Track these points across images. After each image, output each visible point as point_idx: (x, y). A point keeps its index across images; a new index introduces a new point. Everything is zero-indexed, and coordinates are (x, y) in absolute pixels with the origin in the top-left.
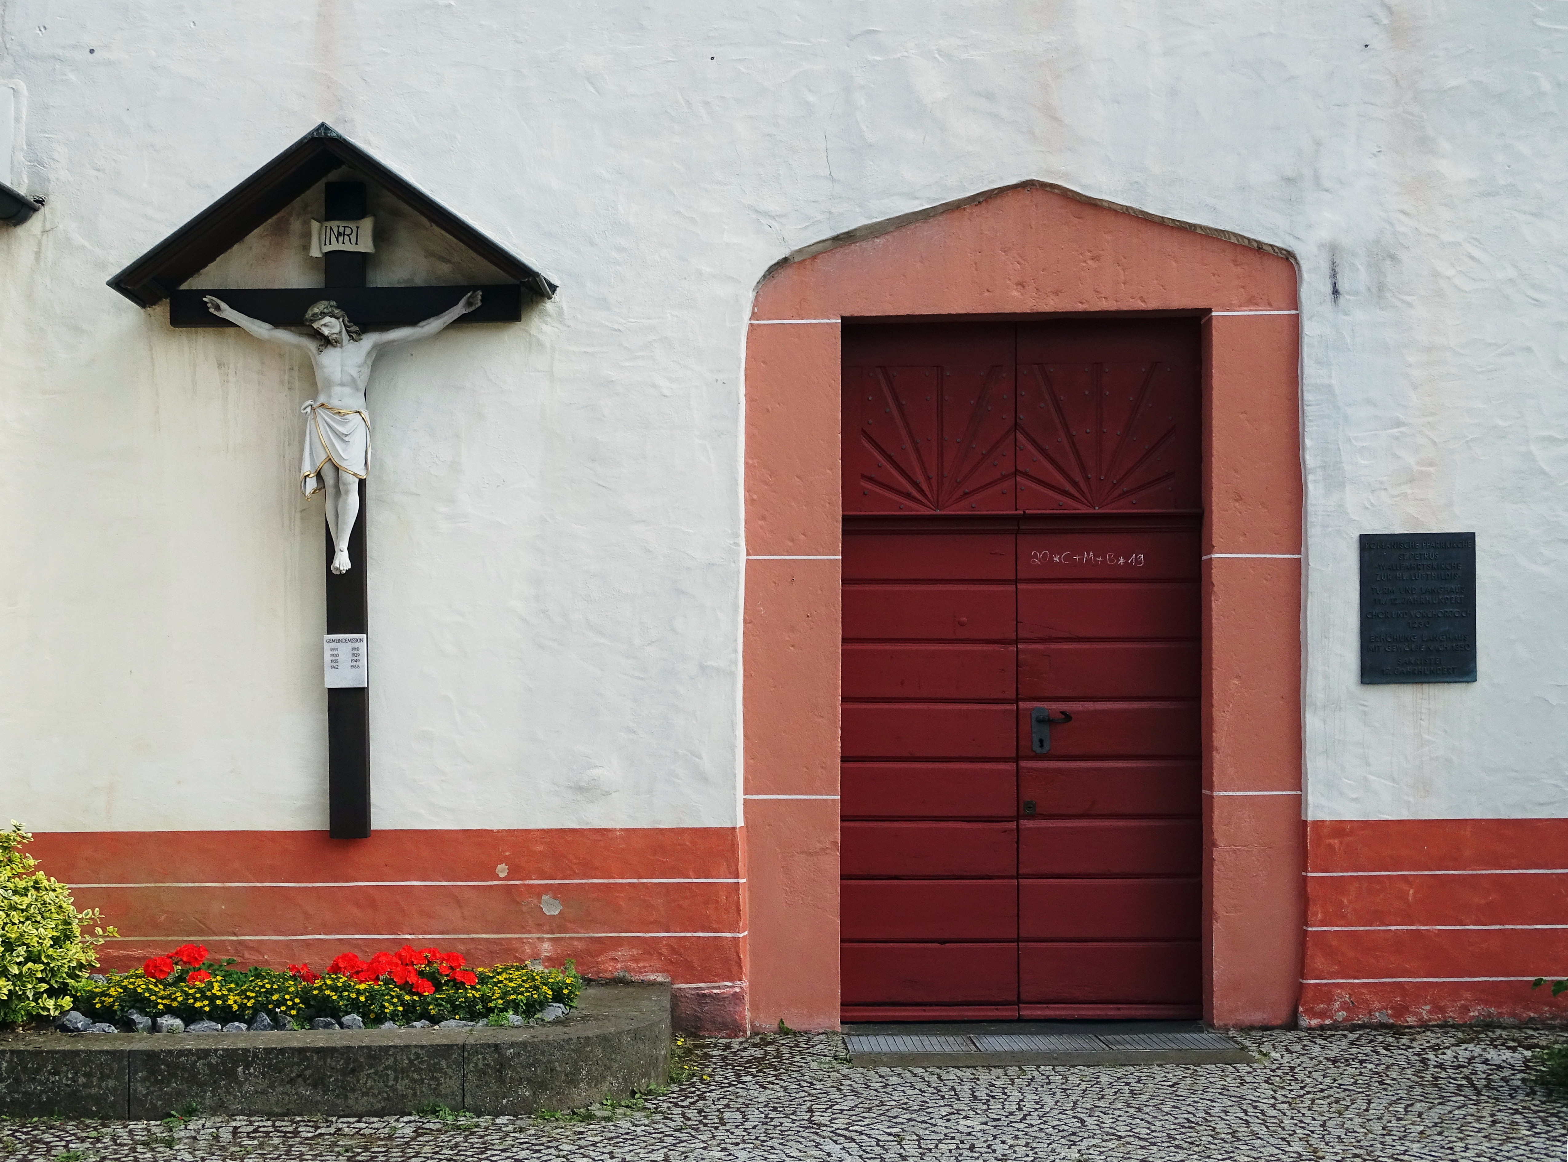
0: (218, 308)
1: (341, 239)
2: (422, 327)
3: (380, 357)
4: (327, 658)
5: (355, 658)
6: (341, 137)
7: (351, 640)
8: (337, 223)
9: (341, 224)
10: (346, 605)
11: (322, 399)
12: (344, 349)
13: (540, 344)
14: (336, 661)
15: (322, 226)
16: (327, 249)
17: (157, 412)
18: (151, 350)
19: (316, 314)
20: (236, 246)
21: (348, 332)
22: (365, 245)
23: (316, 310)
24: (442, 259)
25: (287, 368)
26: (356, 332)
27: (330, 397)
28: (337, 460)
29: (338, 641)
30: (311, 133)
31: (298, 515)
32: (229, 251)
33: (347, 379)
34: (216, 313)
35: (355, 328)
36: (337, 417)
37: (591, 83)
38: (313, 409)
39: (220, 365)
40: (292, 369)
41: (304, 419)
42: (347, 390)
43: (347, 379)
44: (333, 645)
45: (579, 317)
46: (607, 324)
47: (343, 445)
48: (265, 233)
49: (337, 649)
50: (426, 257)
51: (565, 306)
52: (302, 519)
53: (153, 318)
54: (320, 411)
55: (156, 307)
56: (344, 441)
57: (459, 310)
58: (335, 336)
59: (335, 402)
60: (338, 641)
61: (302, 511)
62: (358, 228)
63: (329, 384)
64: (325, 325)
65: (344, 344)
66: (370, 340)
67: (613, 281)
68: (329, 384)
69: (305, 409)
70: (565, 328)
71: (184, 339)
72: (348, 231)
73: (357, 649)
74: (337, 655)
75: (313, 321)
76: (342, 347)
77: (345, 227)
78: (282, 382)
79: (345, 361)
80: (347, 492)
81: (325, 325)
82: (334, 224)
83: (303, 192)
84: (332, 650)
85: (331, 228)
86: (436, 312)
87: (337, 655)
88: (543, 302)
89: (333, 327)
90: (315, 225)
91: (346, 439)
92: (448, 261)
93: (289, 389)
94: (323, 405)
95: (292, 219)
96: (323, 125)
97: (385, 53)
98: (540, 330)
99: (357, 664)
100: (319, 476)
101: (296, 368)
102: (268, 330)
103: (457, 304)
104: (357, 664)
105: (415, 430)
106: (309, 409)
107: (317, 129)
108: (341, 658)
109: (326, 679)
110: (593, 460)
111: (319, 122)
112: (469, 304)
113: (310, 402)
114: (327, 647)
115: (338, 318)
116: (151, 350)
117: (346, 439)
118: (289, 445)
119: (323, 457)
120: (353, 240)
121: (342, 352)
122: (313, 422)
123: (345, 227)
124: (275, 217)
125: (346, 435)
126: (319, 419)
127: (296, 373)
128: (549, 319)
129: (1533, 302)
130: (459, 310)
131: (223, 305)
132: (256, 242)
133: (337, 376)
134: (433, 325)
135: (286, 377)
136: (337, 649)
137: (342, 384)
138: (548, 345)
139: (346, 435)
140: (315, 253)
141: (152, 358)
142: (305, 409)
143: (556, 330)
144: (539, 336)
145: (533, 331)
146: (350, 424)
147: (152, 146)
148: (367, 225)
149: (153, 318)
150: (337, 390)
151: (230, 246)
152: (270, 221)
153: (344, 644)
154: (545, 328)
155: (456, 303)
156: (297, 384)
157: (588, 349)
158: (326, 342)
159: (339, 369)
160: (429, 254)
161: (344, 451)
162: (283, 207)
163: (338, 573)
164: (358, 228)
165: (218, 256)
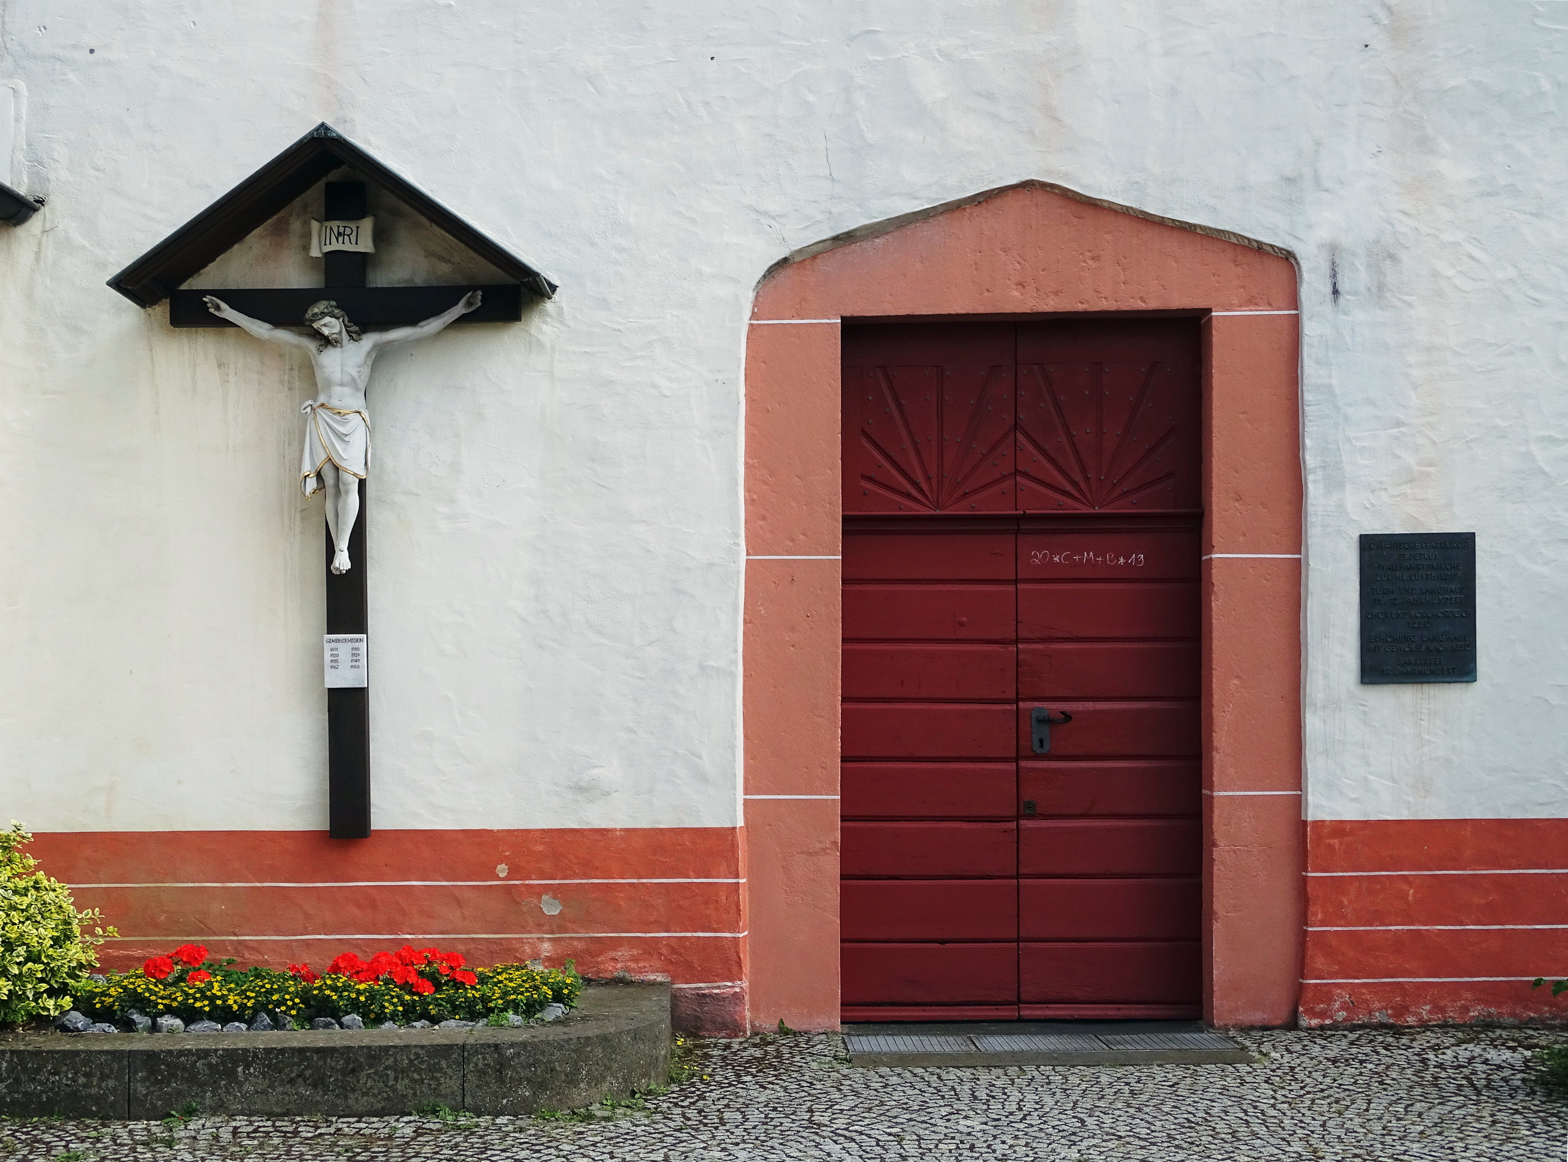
0: (218, 308)
1: (341, 239)
2: (422, 327)
3: (380, 357)
4: (327, 658)
5: (355, 658)
6: (341, 137)
7: (351, 640)
8: (337, 223)
9: (341, 224)
10: (346, 605)
11: (322, 399)
12: (344, 349)
13: (540, 344)
14: (336, 661)
15: (322, 226)
16: (327, 249)
17: (157, 412)
18: (151, 350)
19: (316, 314)
20: (236, 246)
21: (348, 332)
22: (365, 245)
23: (316, 310)
24: (442, 259)
25: (287, 368)
26: (356, 332)
27: (330, 397)
28: (337, 460)
29: (338, 641)
30: (311, 133)
31: (298, 515)
32: (229, 251)
33: (347, 379)
34: (216, 313)
35: (355, 328)
36: (337, 417)
37: (591, 83)
38: (313, 409)
39: (220, 365)
40: (292, 369)
41: (304, 419)
42: (347, 390)
43: (347, 379)
44: (333, 645)
45: (579, 317)
46: (607, 324)
47: (343, 445)
48: (265, 233)
49: (337, 649)
50: (426, 257)
51: (565, 306)
52: (302, 519)
53: (153, 318)
54: (320, 411)
55: (156, 307)
56: (344, 441)
57: (459, 310)
58: (335, 336)
59: (335, 402)
60: (338, 641)
61: (302, 511)
62: (358, 228)
63: (329, 384)
64: (325, 325)
65: (344, 344)
66: (370, 340)
67: (613, 281)
68: (329, 384)
69: (305, 409)
70: (565, 328)
71: (184, 339)
72: (348, 231)
73: (357, 649)
74: (337, 655)
75: (313, 321)
76: (342, 347)
77: (345, 227)
78: (282, 382)
79: (345, 361)
80: (347, 492)
81: (325, 325)
82: (334, 224)
83: (303, 192)
84: (332, 650)
85: (331, 228)
86: (436, 312)
87: (337, 655)
88: (543, 302)
89: (333, 327)
90: (315, 225)
91: (346, 439)
92: (448, 261)
93: (289, 389)
94: (323, 405)
95: (292, 219)
96: (323, 125)
97: (385, 53)
98: (540, 330)
99: (357, 664)
100: (319, 476)
101: (296, 368)
102: (268, 330)
103: (457, 304)
104: (357, 664)
105: (415, 430)
106: (309, 409)
107: (317, 129)
108: (341, 658)
109: (326, 679)
110: (593, 460)
111: (319, 122)
112: (469, 304)
113: (310, 402)
114: (327, 647)
115: (338, 318)
116: (151, 350)
117: (346, 439)
118: (289, 445)
119: (323, 457)
120: (353, 240)
121: (342, 352)
122: (313, 422)
123: (345, 227)
124: (275, 217)
125: (346, 435)
126: (319, 419)
127: (296, 373)
128: (549, 319)
129: (1533, 302)
130: (459, 310)
131: (223, 305)
132: (256, 242)
133: (337, 376)
134: (433, 325)
135: (286, 377)
136: (337, 649)
137: (342, 384)
138: (548, 345)
139: (346, 435)
140: (315, 253)
141: (152, 358)
142: (305, 409)
143: (556, 330)
144: (539, 336)
145: (533, 331)
146: (350, 424)
147: (152, 146)
148: (367, 225)
149: (153, 318)
150: (337, 390)
151: (230, 246)
152: (270, 221)
153: (344, 644)
154: (545, 328)
155: (456, 303)
156: (297, 384)
157: (588, 349)
158: (326, 342)
159: (339, 369)
160: (429, 254)
161: (344, 451)
162: (283, 207)
163: (338, 573)
164: (358, 228)
165: (218, 256)
